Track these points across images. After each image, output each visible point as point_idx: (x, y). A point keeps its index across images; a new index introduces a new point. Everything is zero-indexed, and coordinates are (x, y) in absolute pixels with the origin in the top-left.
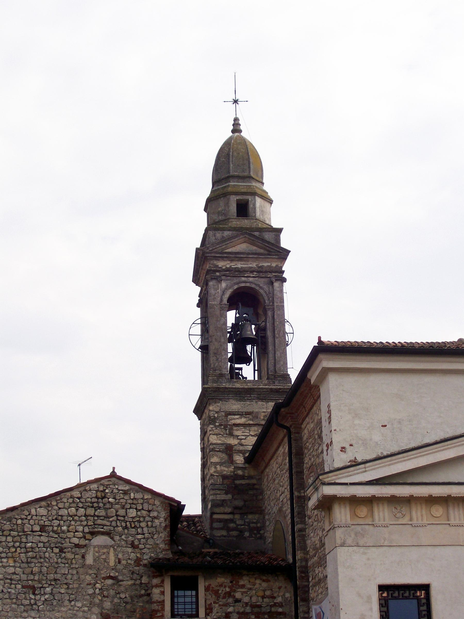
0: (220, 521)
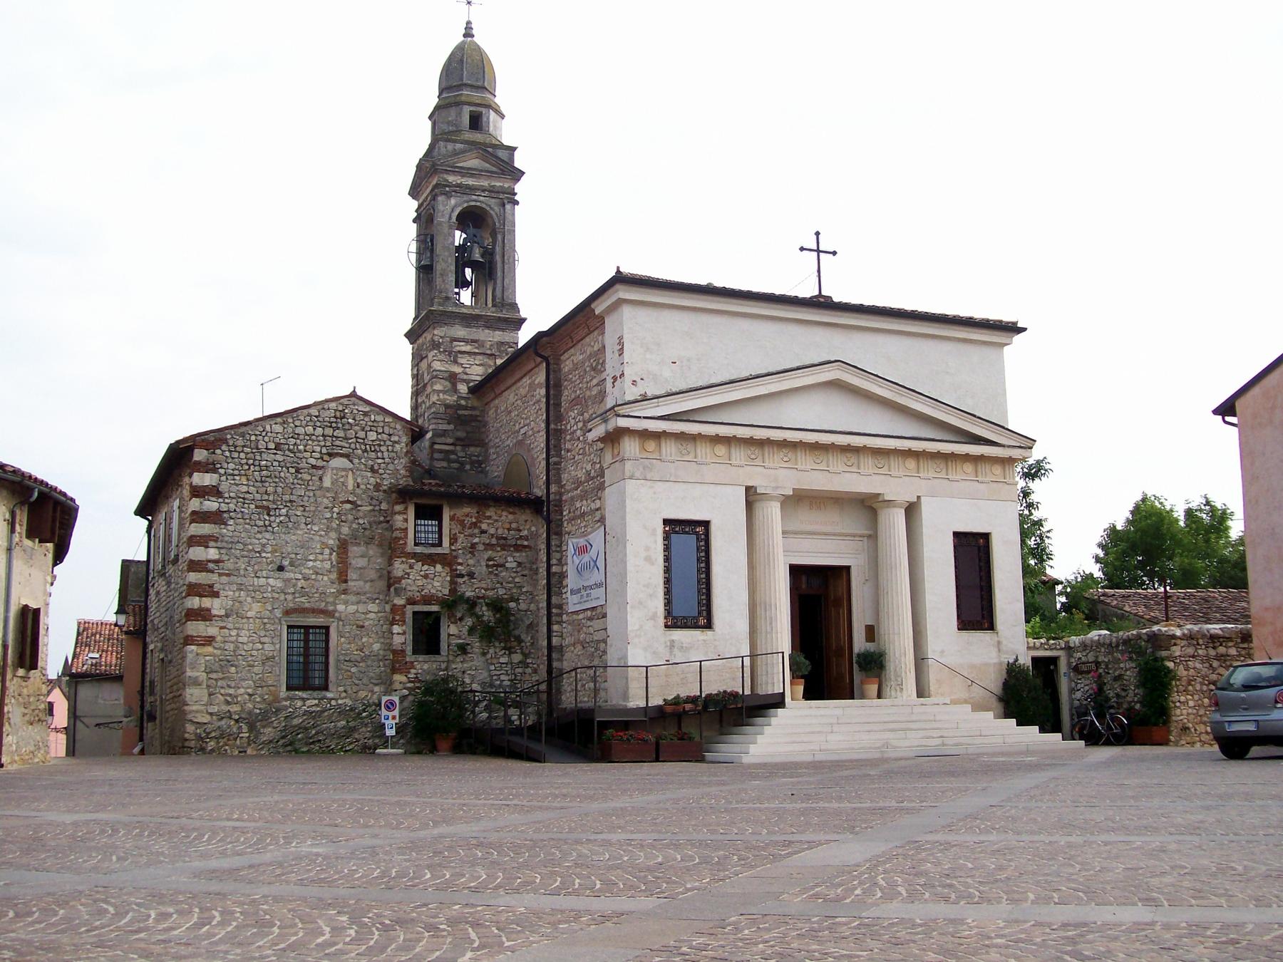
0: (441, 451)
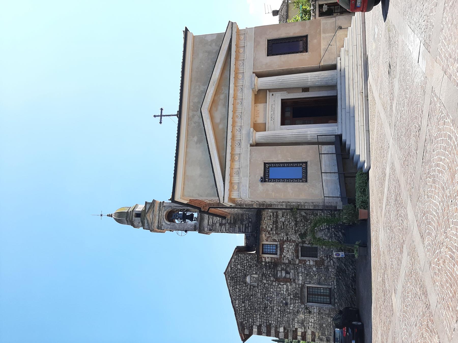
0: (245, 229)
